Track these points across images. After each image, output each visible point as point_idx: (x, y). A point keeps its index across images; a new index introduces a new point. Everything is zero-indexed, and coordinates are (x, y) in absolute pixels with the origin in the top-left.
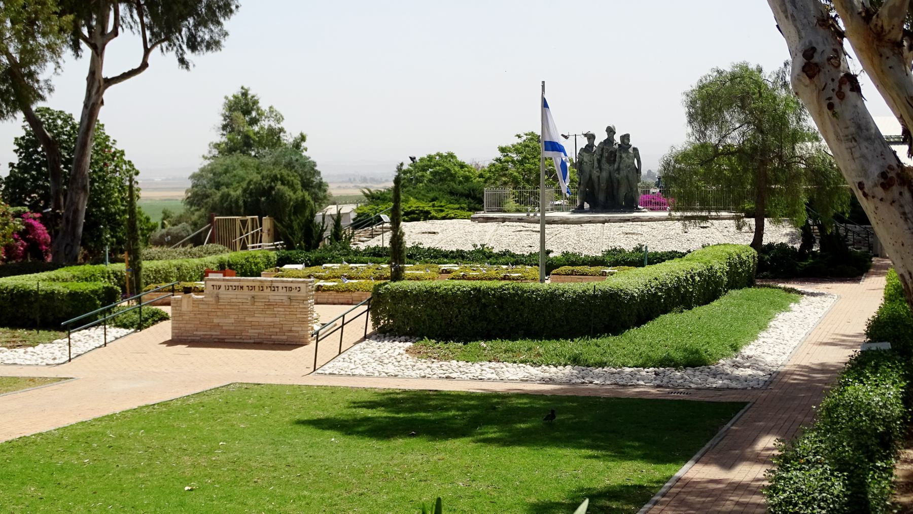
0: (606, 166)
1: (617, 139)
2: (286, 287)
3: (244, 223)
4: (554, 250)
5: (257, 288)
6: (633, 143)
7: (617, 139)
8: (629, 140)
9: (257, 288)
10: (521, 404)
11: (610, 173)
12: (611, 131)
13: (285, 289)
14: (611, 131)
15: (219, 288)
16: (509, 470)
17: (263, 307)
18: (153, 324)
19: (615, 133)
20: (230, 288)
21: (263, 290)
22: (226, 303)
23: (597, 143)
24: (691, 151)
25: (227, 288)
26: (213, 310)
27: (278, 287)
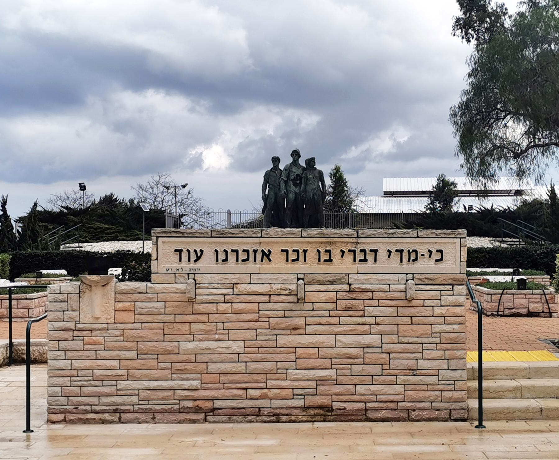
0: (293, 188)
1: (302, 162)
2: (401, 251)
4: (34, 431)
5: (312, 255)
7: (302, 162)
9: (312, 255)
11: (296, 193)
13: (395, 257)
14: (296, 154)
15: (198, 258)
16: (543, 87)
17: (330, 306)
19: (300, 156)
20: (232, 258)
21: (330, 260)
22: (221, 298)
23: (282, 167)
25: (222, 256)
26: (179, 318)
27: (376, 251)
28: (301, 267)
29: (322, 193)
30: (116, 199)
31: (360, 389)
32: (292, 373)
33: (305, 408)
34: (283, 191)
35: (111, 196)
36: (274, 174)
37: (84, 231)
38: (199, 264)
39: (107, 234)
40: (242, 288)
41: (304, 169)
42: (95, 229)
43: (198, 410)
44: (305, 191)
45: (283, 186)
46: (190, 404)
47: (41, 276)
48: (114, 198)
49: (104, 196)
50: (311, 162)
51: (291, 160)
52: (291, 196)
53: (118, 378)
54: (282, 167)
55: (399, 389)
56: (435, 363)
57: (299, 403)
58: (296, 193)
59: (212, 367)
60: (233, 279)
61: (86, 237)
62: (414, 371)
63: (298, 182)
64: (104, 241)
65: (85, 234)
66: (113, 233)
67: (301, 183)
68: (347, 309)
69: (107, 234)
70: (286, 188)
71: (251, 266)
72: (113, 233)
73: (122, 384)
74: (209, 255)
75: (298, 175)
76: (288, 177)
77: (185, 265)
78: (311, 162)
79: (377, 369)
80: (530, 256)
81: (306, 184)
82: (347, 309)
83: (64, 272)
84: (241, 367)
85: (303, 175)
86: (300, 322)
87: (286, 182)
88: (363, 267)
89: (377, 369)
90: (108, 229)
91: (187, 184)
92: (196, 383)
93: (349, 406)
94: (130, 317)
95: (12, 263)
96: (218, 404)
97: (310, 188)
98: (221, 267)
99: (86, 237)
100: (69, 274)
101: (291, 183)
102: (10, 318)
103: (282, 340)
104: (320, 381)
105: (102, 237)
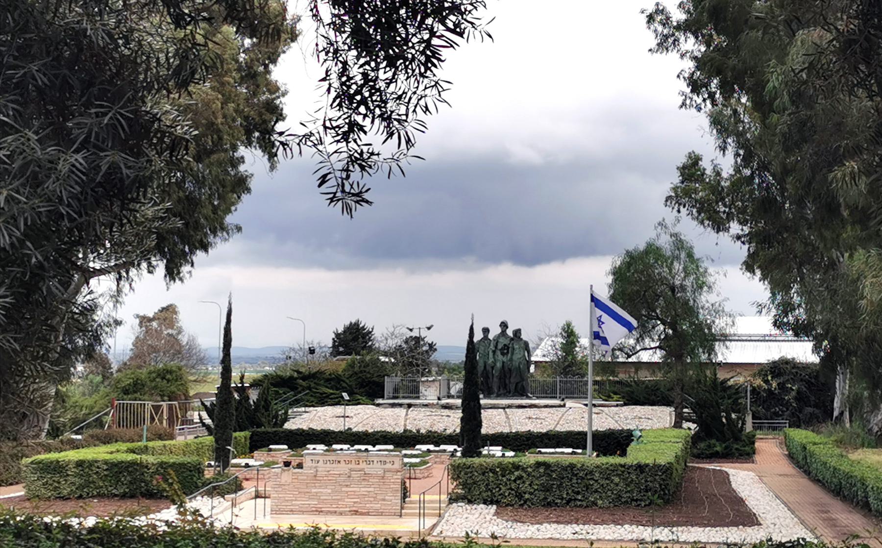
0: (500, 357)
1: (510, 332)
3: (157, 408)
5: (353, 462)
6: (524, 336)
7: (510, 332)
8: (520, 333)
9: (353, 462)
10: (176, 412)
11: (503, 362)
12: (504, 325)
13: (379, 463)
14: (504, 325)
18: (700, 542)
19: (507, 327)
24: (136, 200)
28: (350, 466)
29: (528, 361)
30: (363, 327)
31: (367, 505)
32: (346, 500)
33: (350, 511)
34: (491, 360)
35: (357, 324)
36: (483, 344)
37: (312, 396)
38: (318, 465)
39: (332, 399)
40: (331, 472)
41: (512, 339)
42: (321, 394)
43: (317, 511)
44: (511, 360)
45: (491, 354)
46: (314, 509)
47: (270, 450)
48: (361, 326)
49: (349, 323)
50: (517, 333)
51: (499, 330)
52: (499, 365)
53: (292, 500)
54: (491, 336)
55: (379, 505)
56: (391, 498)
57: (348, 509)
58: (503, 362)
59: (322, 498)
60: (328, 469)
61: (312, 402)
62: (384, 500)
63: (505, 351)
64: (329, 405)
65: (312, 399)
66: (337, 398)
67: (508, 352)
68: (364, 480)
69: (332, 399)
70: (494, 357)
71: (334, 465)
72: (337, 398)
73: (294, 502)
74: (321, 462)
75: (505, 345)
76: (496, 347)
77: (314, 465)
78: (517, 333)
79: (372, 499)
80: (616, 438)
81: (513, 354)
82: (364, 480)
83: (285, 447)
84: (330, 498)
85: (511, 345)
86: (349, 483)
87: (494, 352)
88: (369, 466)
89: (372, 499)
90: (332, 394)
91: (432, 326)
92: (316, 503)
93: (363, 511)
94: (296, 481)
95: (251, 438)
96: (323, 509)
97: (515, 357)
98: (325, 465)
99: (312, 402)
100: (289, 448)
101: (498, 353)
102: (258, 479)
103: (343, 489)
104: (355, 503)
105: (327, 402)
